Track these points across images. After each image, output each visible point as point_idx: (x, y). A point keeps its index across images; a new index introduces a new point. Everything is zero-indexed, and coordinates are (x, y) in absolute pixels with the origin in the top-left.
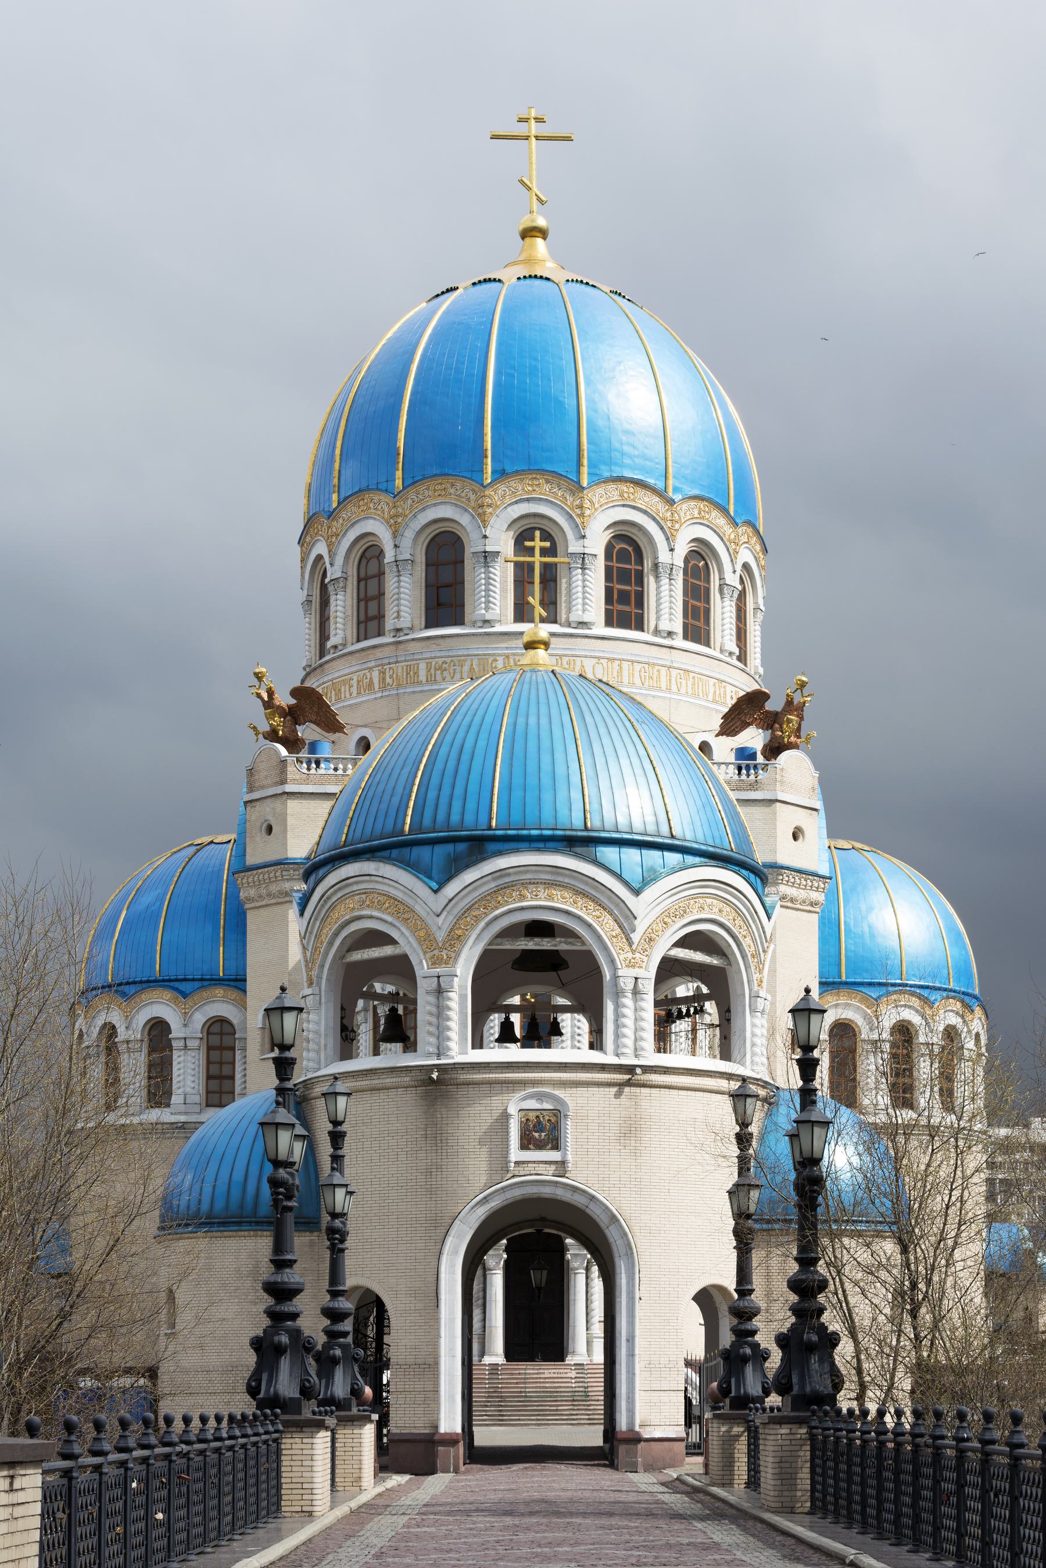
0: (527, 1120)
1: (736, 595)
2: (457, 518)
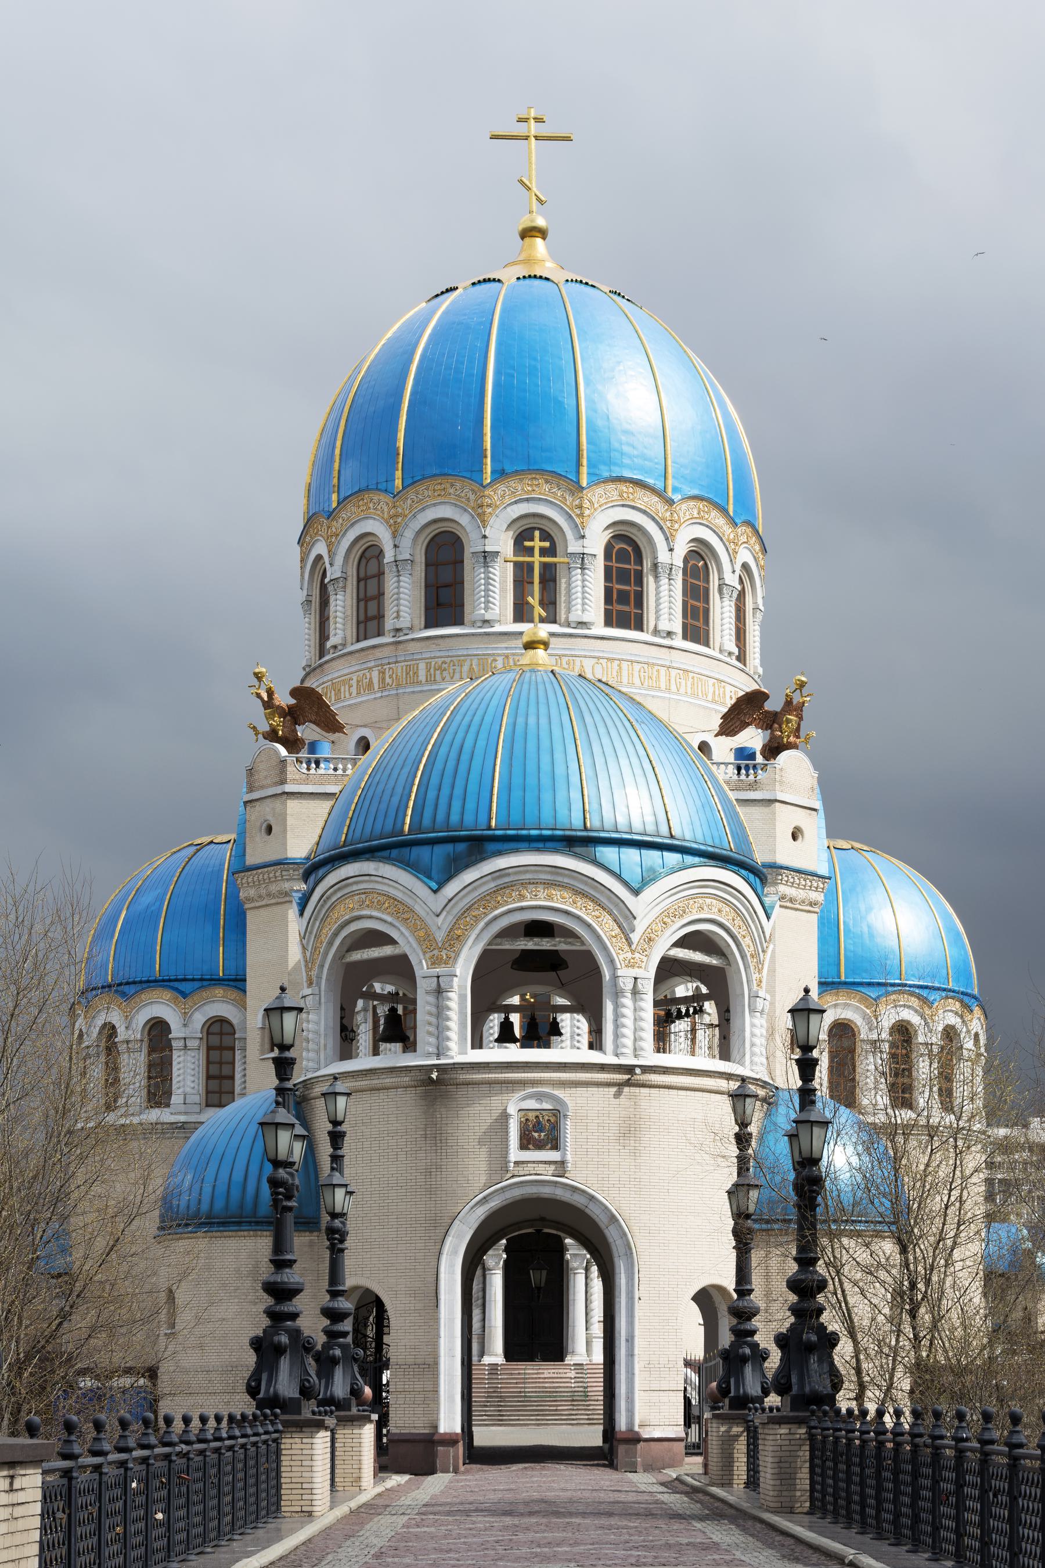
0: (527, 1120)
1: (735, 595)
2: (456, 518)
